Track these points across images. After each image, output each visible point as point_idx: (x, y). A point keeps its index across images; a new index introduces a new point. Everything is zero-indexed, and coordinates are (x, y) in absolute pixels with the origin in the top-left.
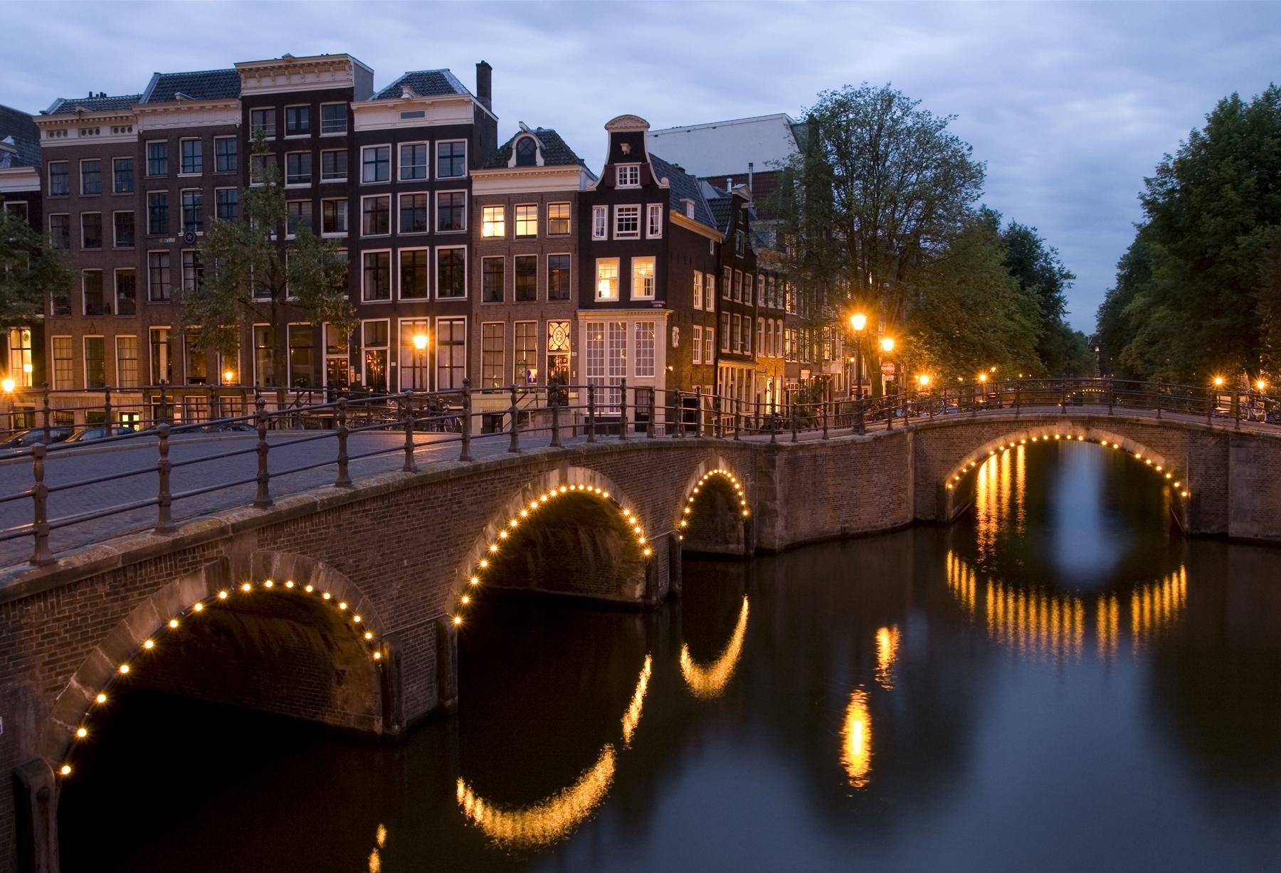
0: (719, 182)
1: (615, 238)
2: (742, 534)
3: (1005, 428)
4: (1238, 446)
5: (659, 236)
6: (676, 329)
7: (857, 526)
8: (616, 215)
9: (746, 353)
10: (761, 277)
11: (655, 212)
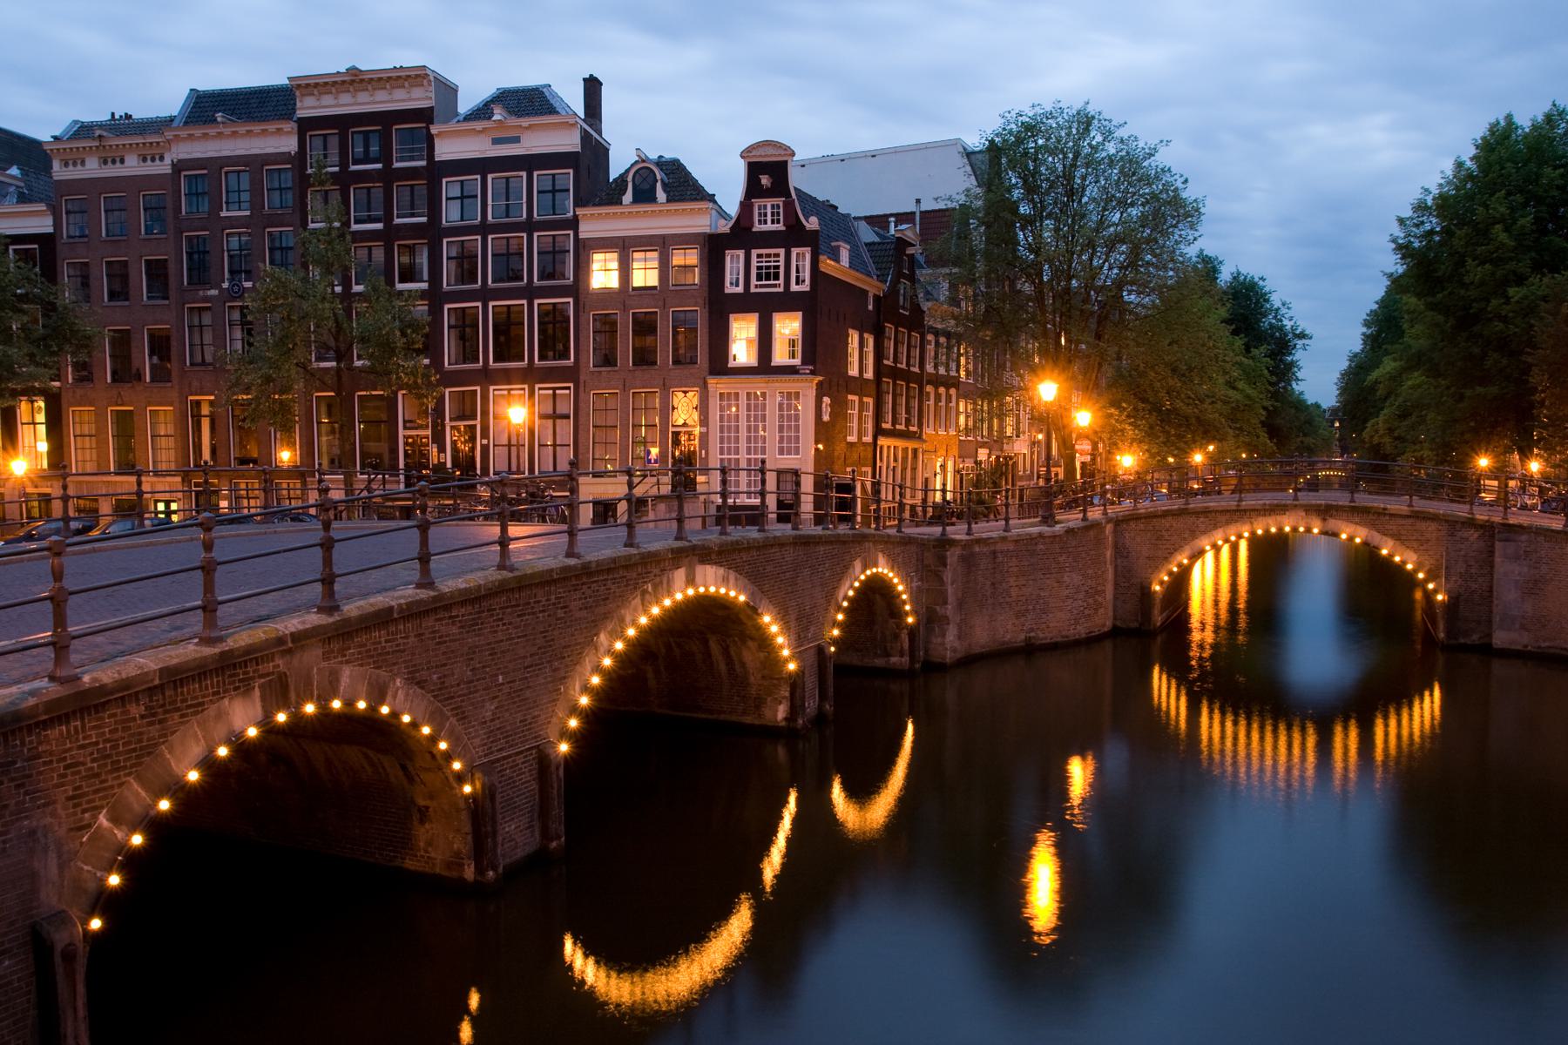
0: (878, 222)
1: (753, 290)
2: (906, 645)
3: (1223, 518)
5: (806, 287)
6: (826, 400)
10: (930, 337)
11: (802, 258)
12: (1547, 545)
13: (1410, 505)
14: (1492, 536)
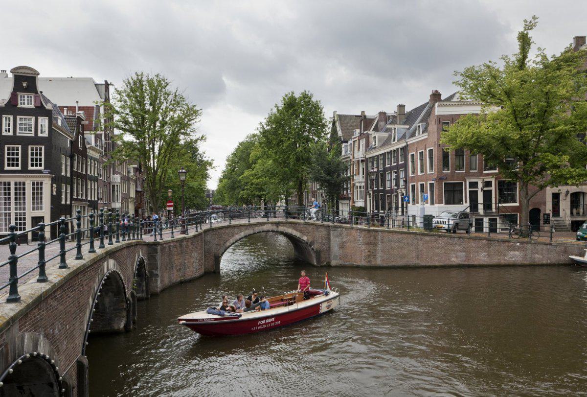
0: (71, 109)
1: (18, 134)
2: (145, 288)
3: (244, 228)
4: (334, 231)
5: (46, 135)
6: (55, 185)
7: (188, 277)
8: (18, 122)
9: (79, 197)
10: (89, 160)
11: (44, 121)
12: (346, 231)
13: (249, 221)
14: (329, 230)
